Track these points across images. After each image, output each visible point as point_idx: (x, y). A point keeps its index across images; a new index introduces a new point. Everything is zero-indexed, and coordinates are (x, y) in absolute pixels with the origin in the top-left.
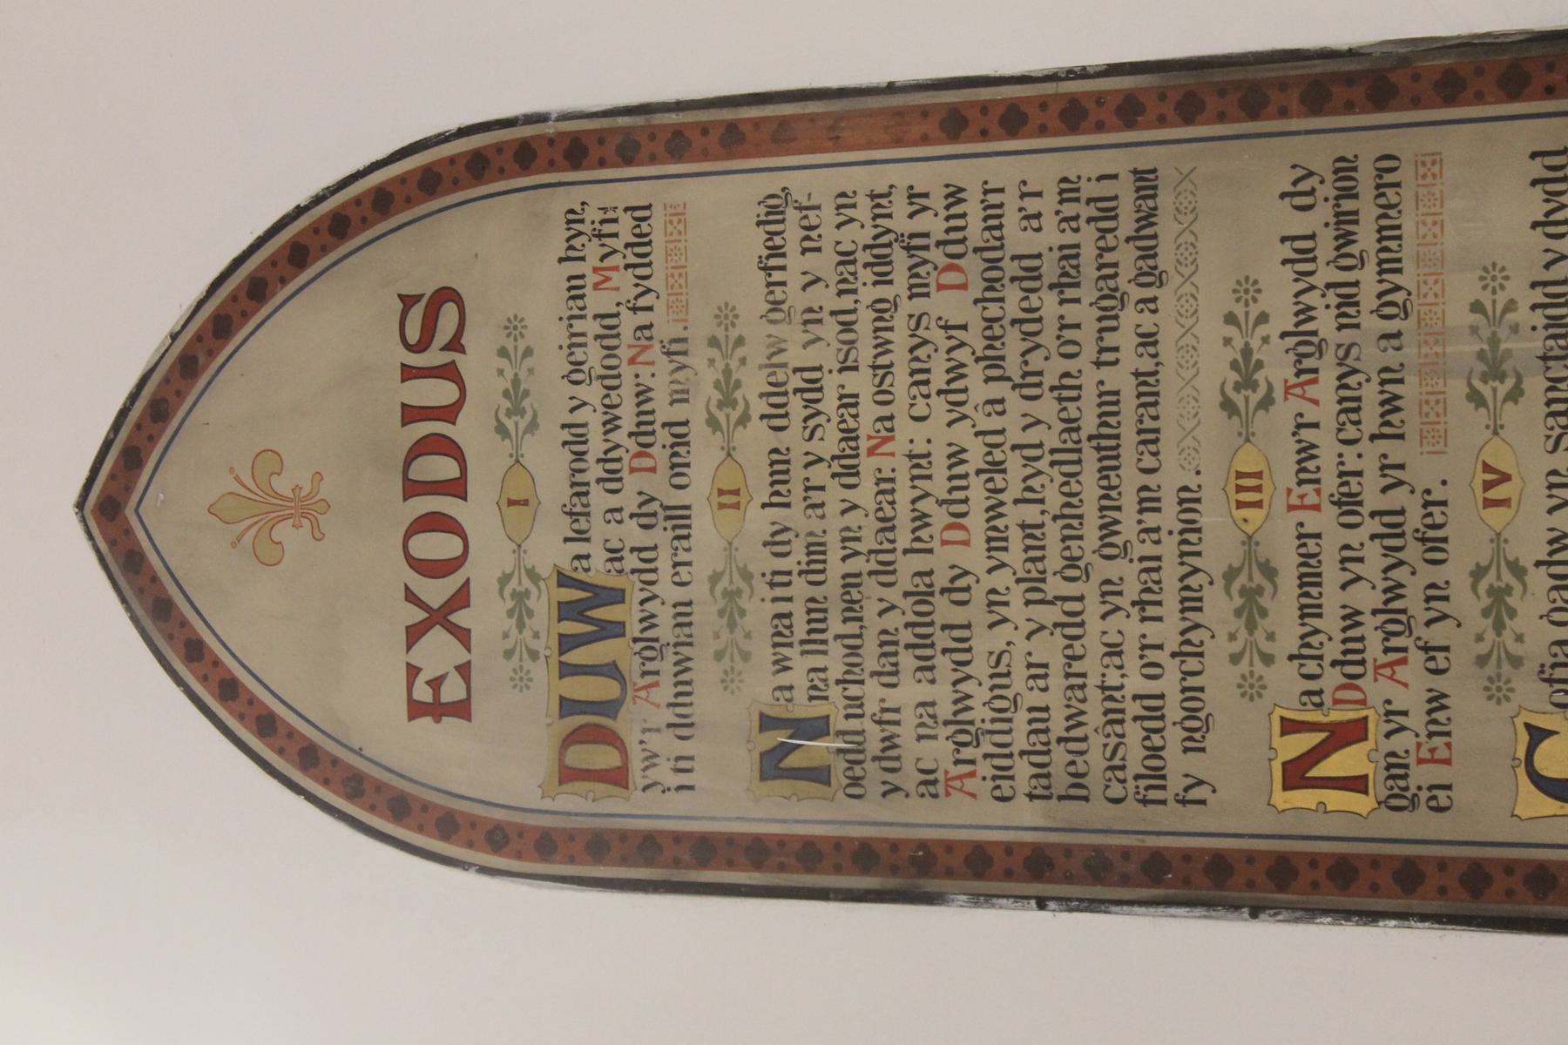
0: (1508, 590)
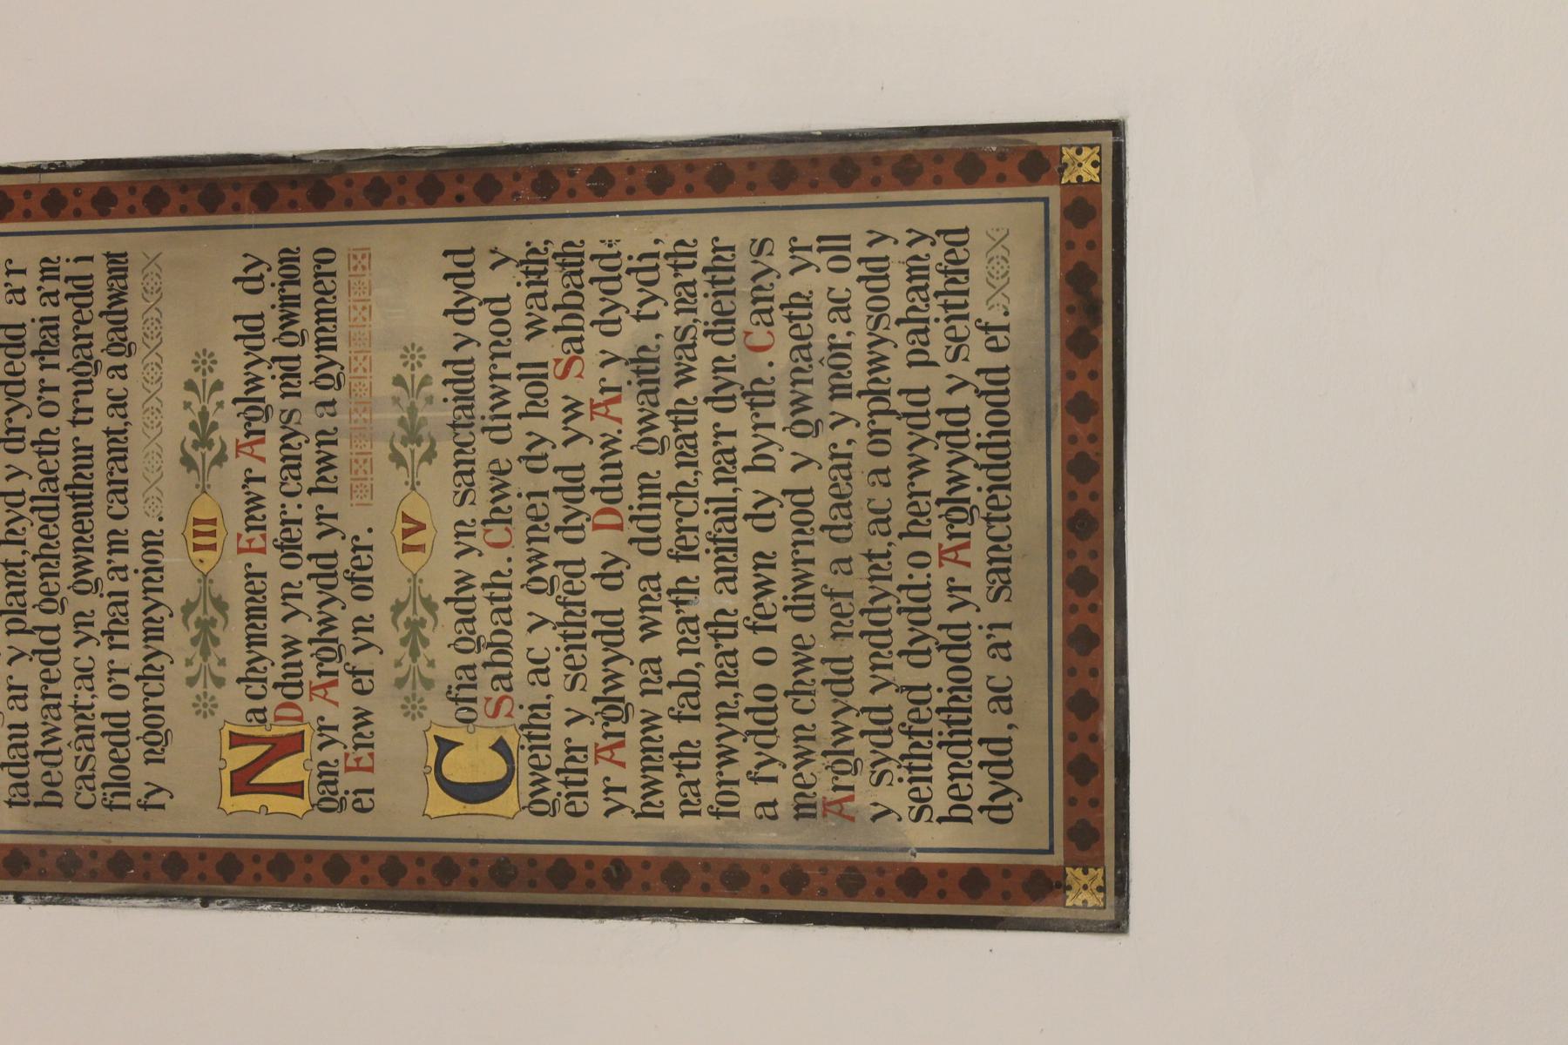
0: (423, 622)
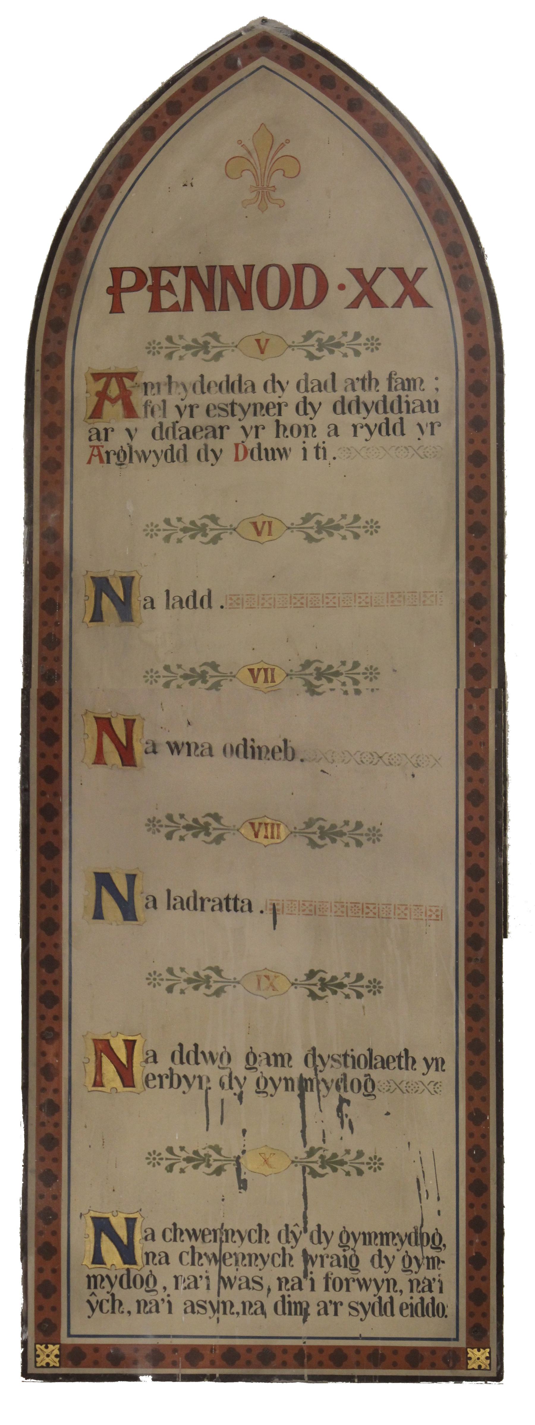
0: (205, 535)
